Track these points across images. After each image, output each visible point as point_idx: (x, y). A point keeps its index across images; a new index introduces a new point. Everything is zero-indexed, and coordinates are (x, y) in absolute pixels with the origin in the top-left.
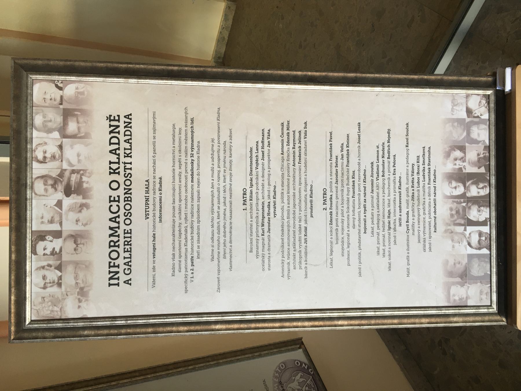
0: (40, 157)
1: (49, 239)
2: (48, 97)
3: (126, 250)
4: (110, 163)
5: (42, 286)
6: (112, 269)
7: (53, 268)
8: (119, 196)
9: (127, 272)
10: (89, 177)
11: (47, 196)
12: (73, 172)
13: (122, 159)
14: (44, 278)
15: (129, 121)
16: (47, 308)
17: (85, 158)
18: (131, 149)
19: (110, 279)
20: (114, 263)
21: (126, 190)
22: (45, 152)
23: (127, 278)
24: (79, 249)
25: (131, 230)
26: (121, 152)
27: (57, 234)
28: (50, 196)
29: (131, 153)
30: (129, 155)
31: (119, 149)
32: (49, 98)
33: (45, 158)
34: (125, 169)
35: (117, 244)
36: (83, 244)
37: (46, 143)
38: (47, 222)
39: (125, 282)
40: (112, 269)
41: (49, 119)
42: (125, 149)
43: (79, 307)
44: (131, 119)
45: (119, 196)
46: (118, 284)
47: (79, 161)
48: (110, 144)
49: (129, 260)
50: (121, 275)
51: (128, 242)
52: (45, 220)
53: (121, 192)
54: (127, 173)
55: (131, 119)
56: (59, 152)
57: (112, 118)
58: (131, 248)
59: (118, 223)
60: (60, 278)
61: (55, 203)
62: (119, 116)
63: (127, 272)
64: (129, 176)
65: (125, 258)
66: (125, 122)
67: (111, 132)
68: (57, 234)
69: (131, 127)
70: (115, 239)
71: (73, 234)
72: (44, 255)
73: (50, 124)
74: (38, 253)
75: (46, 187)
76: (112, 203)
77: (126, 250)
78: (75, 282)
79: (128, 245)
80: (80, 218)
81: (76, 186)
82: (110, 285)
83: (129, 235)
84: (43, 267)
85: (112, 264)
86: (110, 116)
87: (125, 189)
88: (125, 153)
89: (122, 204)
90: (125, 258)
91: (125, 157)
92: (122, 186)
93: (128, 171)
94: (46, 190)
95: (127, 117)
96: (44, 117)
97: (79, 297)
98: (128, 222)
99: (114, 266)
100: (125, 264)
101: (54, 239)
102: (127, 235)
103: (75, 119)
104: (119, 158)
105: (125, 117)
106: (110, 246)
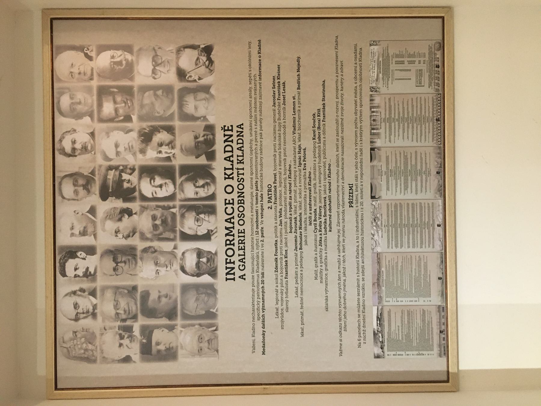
0: (68, 149)
1: (82, 256)
2: (75, 70)
3: (240, 248)
4: (225, 169)
5: (73, 317)
6: (229, 265)
7: (86, 293)
8: (233, 199)
9: (242, 268)
10: (131, 174)
11: (78, 200)
12: (110, 168)
13: (236, 166)
14: (76, 306)
15: (241, 130)
16: (79, 346)
17: (126, 149)
18: (243, 156)
19: (227, 274)
20: (230, 260)
21: (240, 194)
22: (74, 142)
23: (242, 273)
24: (120, 270)
25: (244, 230)
26: (235, 159)
27: (90, 250)
28: (81, 199)
29: (243, 159)
30: (231, 176)
31: (232, 156)
32: (77, 71)
33: (74, 149)
34: (238, 174)
35: (232, 243)
36: (125, 262)
37: (75, 130)
38: (78, 233)
39: (240, 277)
40: (229, 265)
41: (78, 101)
42: (238, 156)
43: (121, 345)
44: (243, 129)
45: (233, 199)
46: (234, 279)
47: (118, 153)
48: (225, 152)
49: (243, 257)
50: (236, 270)
51: (242, 241)
52: (76, 231)
53: (235, 195)
54: (240, 178)
55: (243, 129)
56: (92, 141)
57: (226, 128)
58: (244, 246)
59: (233, 223)
60: (95, 307)
61: (88, 209)
62: (232, 126)
63: (242, 268)
64: (242, 180)
65: (239, 255)
66: (237, 132)
67: (225, 141)
68: (90, 250)
69: (243, 136)
70: (231, 238)
71: (112, 249)
72: (76, 276)
73: (79, 108)
74: (67, 274)
75: (76, 188)
76: (227, 206)
77: (240, 248)
78: (115, 312)
79: (242, 243)
80: (121, 229)
81: (115, 186)
82: (227, 279)
83: (243, 235)
84: (74, 293)
85: (228, 261)
86: (225, 126)
87: (238, 192)
88: (238, 160)
89: (236, 206)
90: (239, 255)
91: (238, 163)
92: (236, 190)
93: (241, 176)
94: (76, 192)
95: (239, 126)
96: (71, 98)
97: (121, 332)
98: (241, 222)
99: (230, 263)
100: (239, 261)
101: (88, 256)
102: (240, 235)
103: (111, 98)
104: (232, 165)
105: (237, 127)
106: (226, 245)
